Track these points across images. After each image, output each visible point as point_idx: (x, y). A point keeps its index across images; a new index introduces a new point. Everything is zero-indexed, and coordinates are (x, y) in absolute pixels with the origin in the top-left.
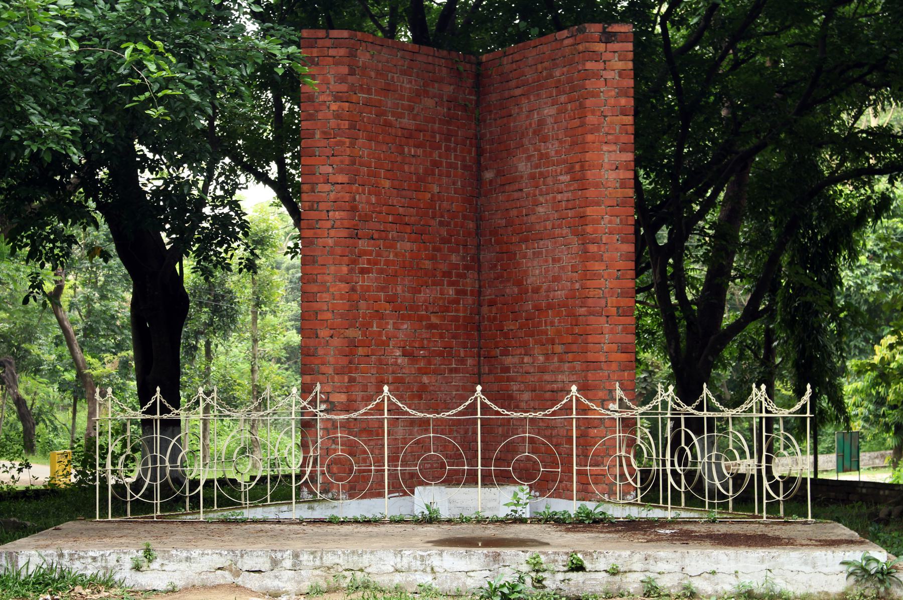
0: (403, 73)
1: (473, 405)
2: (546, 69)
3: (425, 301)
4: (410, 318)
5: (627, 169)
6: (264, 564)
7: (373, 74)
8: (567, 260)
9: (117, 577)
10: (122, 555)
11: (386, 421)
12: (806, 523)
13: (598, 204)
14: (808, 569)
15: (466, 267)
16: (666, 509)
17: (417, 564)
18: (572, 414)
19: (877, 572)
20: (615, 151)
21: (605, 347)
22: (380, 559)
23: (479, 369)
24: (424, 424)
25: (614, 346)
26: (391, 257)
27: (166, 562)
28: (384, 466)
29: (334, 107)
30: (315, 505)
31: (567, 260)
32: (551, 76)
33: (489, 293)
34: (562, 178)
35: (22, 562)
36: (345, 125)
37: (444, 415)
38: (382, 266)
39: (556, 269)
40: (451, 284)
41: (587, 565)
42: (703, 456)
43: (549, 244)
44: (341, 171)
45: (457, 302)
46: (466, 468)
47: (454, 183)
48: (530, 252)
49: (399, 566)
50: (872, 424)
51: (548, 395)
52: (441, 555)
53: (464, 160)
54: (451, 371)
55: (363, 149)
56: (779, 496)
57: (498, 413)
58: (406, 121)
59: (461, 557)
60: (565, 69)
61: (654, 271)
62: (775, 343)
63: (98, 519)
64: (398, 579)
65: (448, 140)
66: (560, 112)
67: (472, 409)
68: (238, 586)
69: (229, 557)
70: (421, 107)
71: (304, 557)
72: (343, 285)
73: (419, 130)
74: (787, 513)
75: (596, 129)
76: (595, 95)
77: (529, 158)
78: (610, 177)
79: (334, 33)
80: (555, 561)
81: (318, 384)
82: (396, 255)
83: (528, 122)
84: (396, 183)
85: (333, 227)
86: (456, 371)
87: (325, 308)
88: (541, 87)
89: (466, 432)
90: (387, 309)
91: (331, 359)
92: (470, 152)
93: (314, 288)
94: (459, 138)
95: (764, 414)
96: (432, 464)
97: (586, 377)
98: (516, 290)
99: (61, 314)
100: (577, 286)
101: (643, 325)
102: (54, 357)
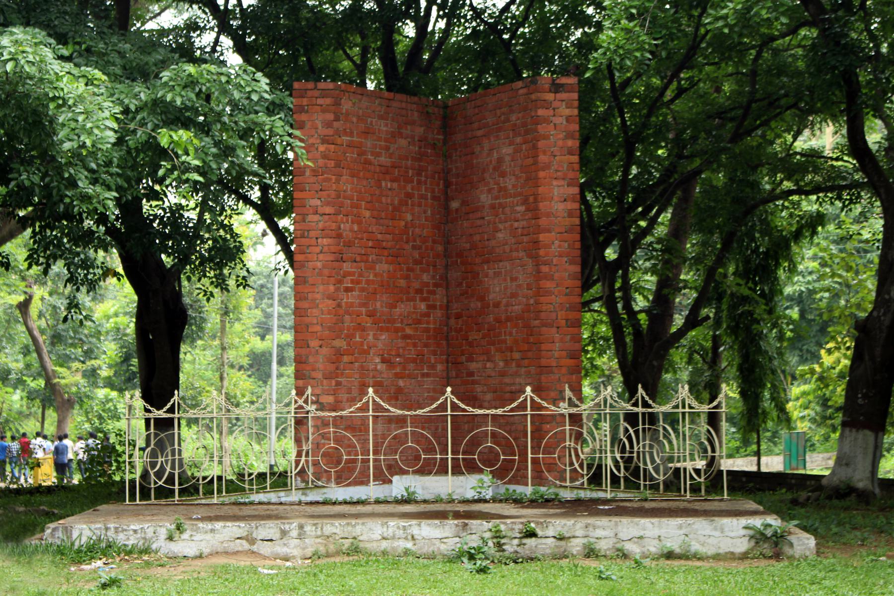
0: (381, 117)
2: (504, 114)
3: (401, 315)
4: (388, 329)
5: (574, 201)
6: (276, 535)
7: (355, 120)
8: (522, 280)
9: (154, 547)
10: (158, 528)
11: (449, 418)
12: (722, 500)
13: (549, 231)
14: (717, 534)
15: (436, 285)
16: (606, 491)
17: (400, 533)
18: (526, 410)
19: (773, 536)
20: (563, 186)
21: (556, 354)
22: (370, 529)
23: (448, 373)
24: (401, 421)
25: (564, 353)
26: (371, 277)
27: (194, 533)
29: (322, 148)
30: (308, 491)
31: (522, 280)
32: (508, 120)
33: (456, 307)
35: (75, 534)
36: (332, 164)
37: (419, 412)
38: (363, 285)
39: (514, 287)
40: (423, 300)
41: (540, 532)
42: (638, 443)
43: (507, 265)
44: (328, 204)
45: (427, 315)
46: (438, 456)
47: (425, 212)
48: (491, 272)
49: (385, 535)
50: (819, 425)
51: (507, 395)
52: (419, 525)
53: (433, 191)
54: (423, 375)
55: (347, 185)
56: (700, 477)
57: (464, 410)
58: (383, 159)
59: (436, 526)
60: (520, 115)
61: (603, 285)
62: (722, 349)
63: (127, 502)
64: (384, 545)
65: (419, 174)
66: (516, 151)
68: (253, 552)
69: (246, 529)
70: (396, 146)
71: (308, 528)
72: (330, 302)
73: (394, 166)
74: (708, 492)
75: (547, 167)
76: (546, 137)
77: (490, 191)
78: (559, 207)
79: (322, 85)
80: (512, 529)
81: (309, 388)
82: (376, 275)
83: (489, 159)
84: (375, 213)
85: (321, 252)
87: (315, 322)
88: (499, 129)
89: (437, 428)
90: (368, 322)
93: (304, 304)
94: (429, 173)
95: (687, 410)
96: (407, 457)
97: (540, 379)
98: (479, 304)
99: (31, 323)
100: (532, 301)
101: (598, 333)
102: (21, 365)
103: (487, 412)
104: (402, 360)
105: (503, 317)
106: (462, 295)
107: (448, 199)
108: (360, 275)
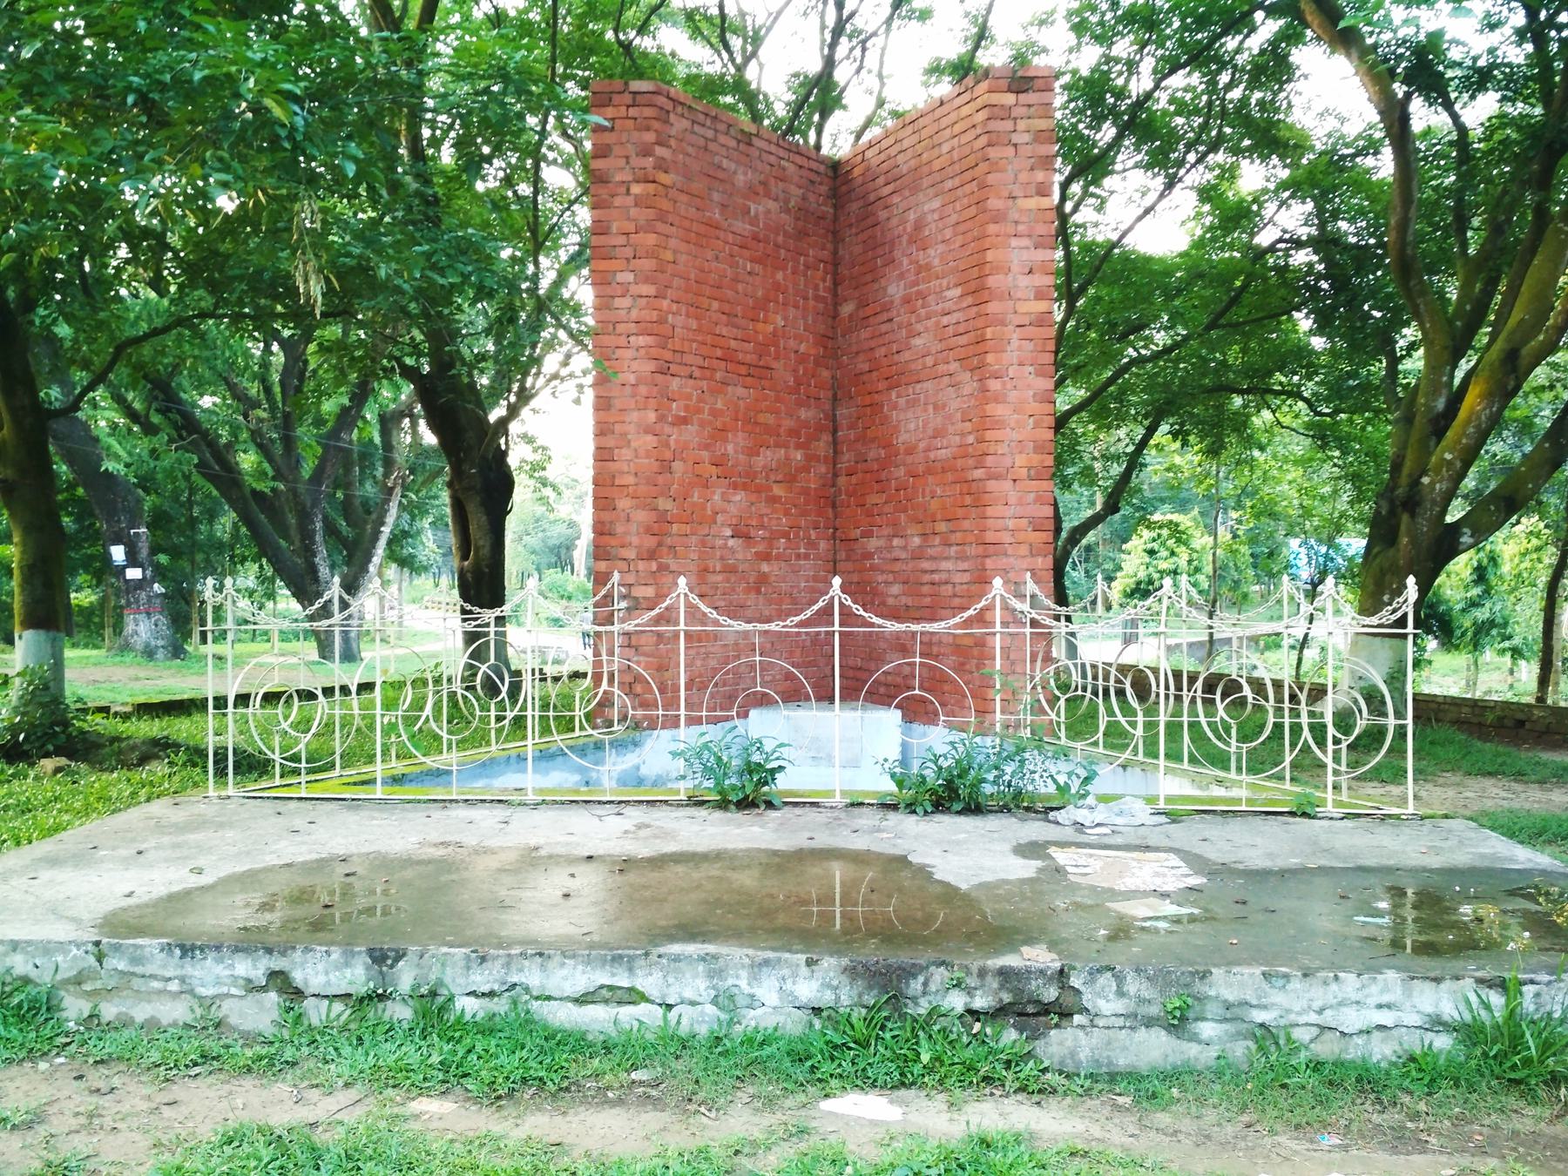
1: (827, 611)
3: (764, 467)
4: (745, 487)
11: (837, 636)
24: (743, 645)
26: (719, 405)
28: (678, 709)
38: (705, 416)
39: (939, 420)
40: (798, 446)
48: (902, 401)
53: (816, 288)
54: (798, 556)
67: (827, 611)
72: (650, 438)
73: (755, 238)
86: (807, 557)
87: (626, 469)
91: (635, 540)
98: (882, 453)
100: (971, 439)
103: (915, 627)
105: (921, 469)
106: (857, 440)
107: (837, 301)
108: (700, 400)
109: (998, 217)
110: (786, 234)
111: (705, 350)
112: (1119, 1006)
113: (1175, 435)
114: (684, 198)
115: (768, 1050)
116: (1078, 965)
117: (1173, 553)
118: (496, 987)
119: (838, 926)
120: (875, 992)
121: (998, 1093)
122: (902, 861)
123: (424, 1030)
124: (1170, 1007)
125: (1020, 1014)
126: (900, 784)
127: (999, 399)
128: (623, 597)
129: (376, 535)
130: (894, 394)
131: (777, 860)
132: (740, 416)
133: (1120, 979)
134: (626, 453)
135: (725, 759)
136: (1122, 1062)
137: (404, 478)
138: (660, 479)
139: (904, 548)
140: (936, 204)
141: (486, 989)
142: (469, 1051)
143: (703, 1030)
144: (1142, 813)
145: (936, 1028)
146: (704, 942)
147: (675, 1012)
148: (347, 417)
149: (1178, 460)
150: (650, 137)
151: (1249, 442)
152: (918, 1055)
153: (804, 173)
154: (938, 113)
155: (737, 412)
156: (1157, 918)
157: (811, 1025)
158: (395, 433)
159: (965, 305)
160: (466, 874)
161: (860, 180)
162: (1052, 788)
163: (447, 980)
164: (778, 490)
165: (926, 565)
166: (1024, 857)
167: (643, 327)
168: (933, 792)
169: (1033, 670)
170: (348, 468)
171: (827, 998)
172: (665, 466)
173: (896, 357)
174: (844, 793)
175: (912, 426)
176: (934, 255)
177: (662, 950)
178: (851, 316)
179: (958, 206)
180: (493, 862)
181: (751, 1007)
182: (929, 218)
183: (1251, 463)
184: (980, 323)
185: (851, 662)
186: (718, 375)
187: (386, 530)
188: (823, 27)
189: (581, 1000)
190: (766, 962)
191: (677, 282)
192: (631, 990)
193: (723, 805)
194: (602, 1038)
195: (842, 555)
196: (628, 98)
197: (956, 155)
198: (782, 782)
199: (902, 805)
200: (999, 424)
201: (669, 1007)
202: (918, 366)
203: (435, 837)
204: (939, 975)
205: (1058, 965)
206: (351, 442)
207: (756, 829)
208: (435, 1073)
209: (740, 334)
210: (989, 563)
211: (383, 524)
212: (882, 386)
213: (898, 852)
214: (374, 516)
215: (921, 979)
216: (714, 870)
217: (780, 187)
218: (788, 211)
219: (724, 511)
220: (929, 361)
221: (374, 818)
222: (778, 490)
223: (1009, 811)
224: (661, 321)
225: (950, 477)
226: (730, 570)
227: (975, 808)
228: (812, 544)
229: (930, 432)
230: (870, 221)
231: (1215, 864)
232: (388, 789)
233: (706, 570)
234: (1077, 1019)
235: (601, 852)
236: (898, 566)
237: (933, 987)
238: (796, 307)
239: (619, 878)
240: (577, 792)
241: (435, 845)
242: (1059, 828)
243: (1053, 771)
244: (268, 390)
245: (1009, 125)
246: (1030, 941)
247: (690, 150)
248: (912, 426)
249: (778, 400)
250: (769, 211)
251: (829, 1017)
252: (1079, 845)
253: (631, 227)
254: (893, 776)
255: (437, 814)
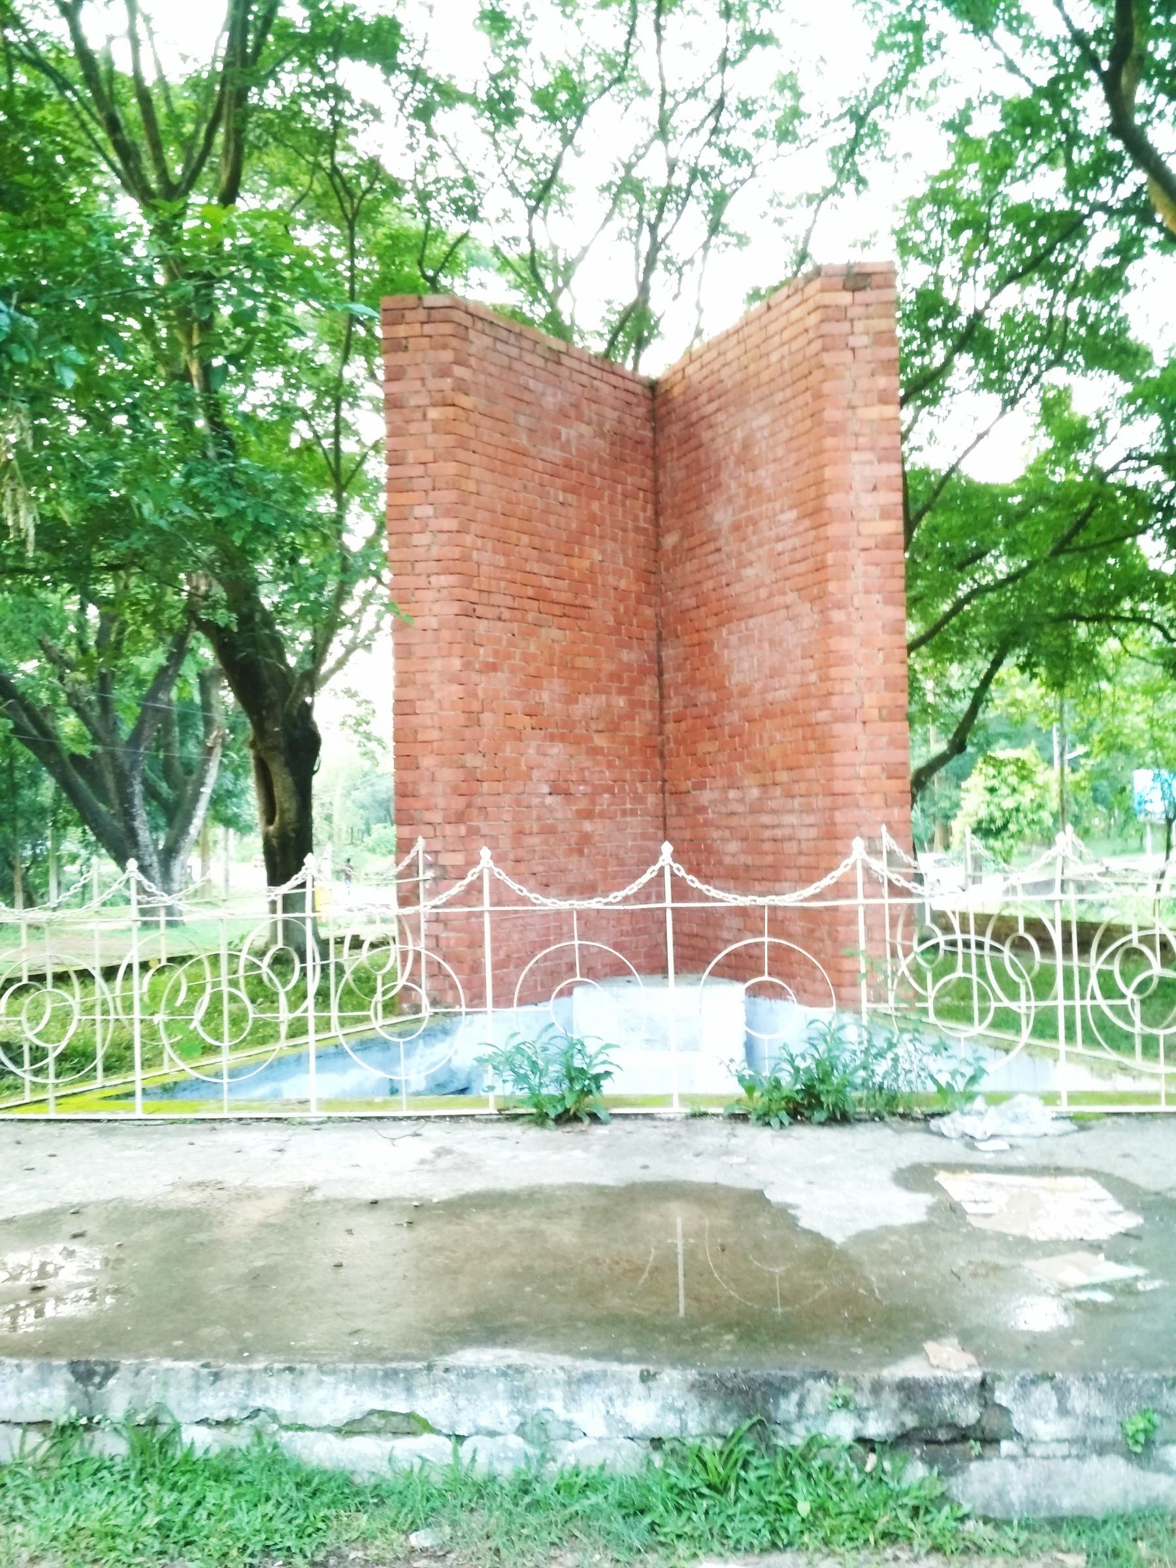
4: (563, 738)
24: (557, 924)
26: (532, 649)
34: (784, 517)
40: (621, 692)
44: (448, 513)
48: (734, 639)
53: (636, 519)
54: (624, 813)
72: (455, 688)
86: (633, 812)
87: (429, 722)
91: (441, 802)
92: (644, 510)
98: (714, 696)
100: (813, 677)
103: (761, 901)
104: (589, 790)
105: (757, 713)
106: (685, 683)
108: (510, 644)
109: (837, 430)
110: (601, 461)
111: (515, 589)
112: (1060, 1428)
113: (1022, 668)
114: (487, 422)
115: (595, 1498)
116: (1005, 1374)
117: (1014, 790)
118: (234, 1414)
119: (682, 1313)
120: (733, 1416)
121: (904, 1556)
122: (756, 1199)
123: (141, 1471)
124: (1130, 1429)
125: (928, 1442)
126: (750, 1090)
127: (844, 631)
128: (430, 866)
129: (197, 795)
130: (724, 631)
131: (603, 1201)
132: (556, 661)
133: (1062, 1392)
134: (430, 706)
135: (541, 1063)
136: (1067, 1503)
137: (223, 737)
138: (467, 733)
139: (741, 801)
140: (765, 419)
141: (220, 1415)
142: (199, 1503)
143: (506, 1470)
144: (1042, 1119)
145: (816, 1464)
146: (505, 1344)
147: (468, 1445)
148: (165, 676)
149: (1019, 694)
150: (447, 356)
151: (1098, 672)
152: (794, 1502)
153: (620, 394)
154: (765, 319)
155: (552, 657)
156: (1094, 1287)
157: (650, 1462)
158: (213, 691)
159: (801, 528)
160: (218, 1233)
161: (681, 399)
162: (932, 1088)
163: (171, 1404)
164: (600, 741)
165: (766, 819)
166: (908, 1188)
167: (445, 566)
168: (788, 1099)
169: (893, 936)
170: (167, 730)
171: (669, 1426)
172: (473, 718)
173: (726, 590)
174: (684, 1099)
175: (746, 666)
176: (765, 476)
177: (449, 1360)
178: (675, 548)
179: (790, 420)
180: (253, 1213)
181: (568, 1438)
182: (759, 435)
183: (1099, 696)
184: (819, 548)
185: (686, 928)
186: (530, 617)
187: (207, 791)
188: (637, 257)
189: (349, 1429)
190: (587, 1378)
191: (481, 515)
192: (409, 1416)
193: (540, 1119)
194: (373, 1481)
195: (672, 809)
196: (421, 314)
197: (786, 364)
198: (608, 1088)
199: (753, 1117)
200: (845, 660)
201: (460, 1439)
202: (751, 598)
203: (193, 1174)
204: (819, 1391)
205: (976, 1375)
206: (170, 702)
207: (578, 1154)
208: (148, 1540)
209: (552, 570)
210: (839, 816)
211: (202, 784)
212: (710, 623)
213: (751, 1185)
214: (194, 777)
215: (794, 1397)
216: (525, 1220)
217: (589, 410)
218: (602, 435)
219: (540, 766)
220: (763, 592)
221: (127, 1147)
222: (600, 741)
223: (882, 1119)
224: (465, 558)
225: (790, 720)
226: (549, 830)
227: (841, 1118)
228: (639, 799)
229: (766, 671)
230: (693, 443)
231: (1147, 1193)
232: (153, 1103)
233: (521, 832)
234: (1006, 1446)
235: (389, 1193)
236: (734, 822)
237: (810, 1408)
238: (614, 539)
239: (406, 1235)
240: (370, 1104)
241: (191, 1187)
242: (944, 1142)
243: (933, 1068)
244: (84, 650)
245: (845, 327)
246: (935, 1332)
247: (492, 369)
248: (746, 666)
249: (596, 641)
250: (581, 436)
251: (673, 1451)
252: (974, 1168)
253: (428, 456)
254: (741, 1079)
255: (203, 1138)
